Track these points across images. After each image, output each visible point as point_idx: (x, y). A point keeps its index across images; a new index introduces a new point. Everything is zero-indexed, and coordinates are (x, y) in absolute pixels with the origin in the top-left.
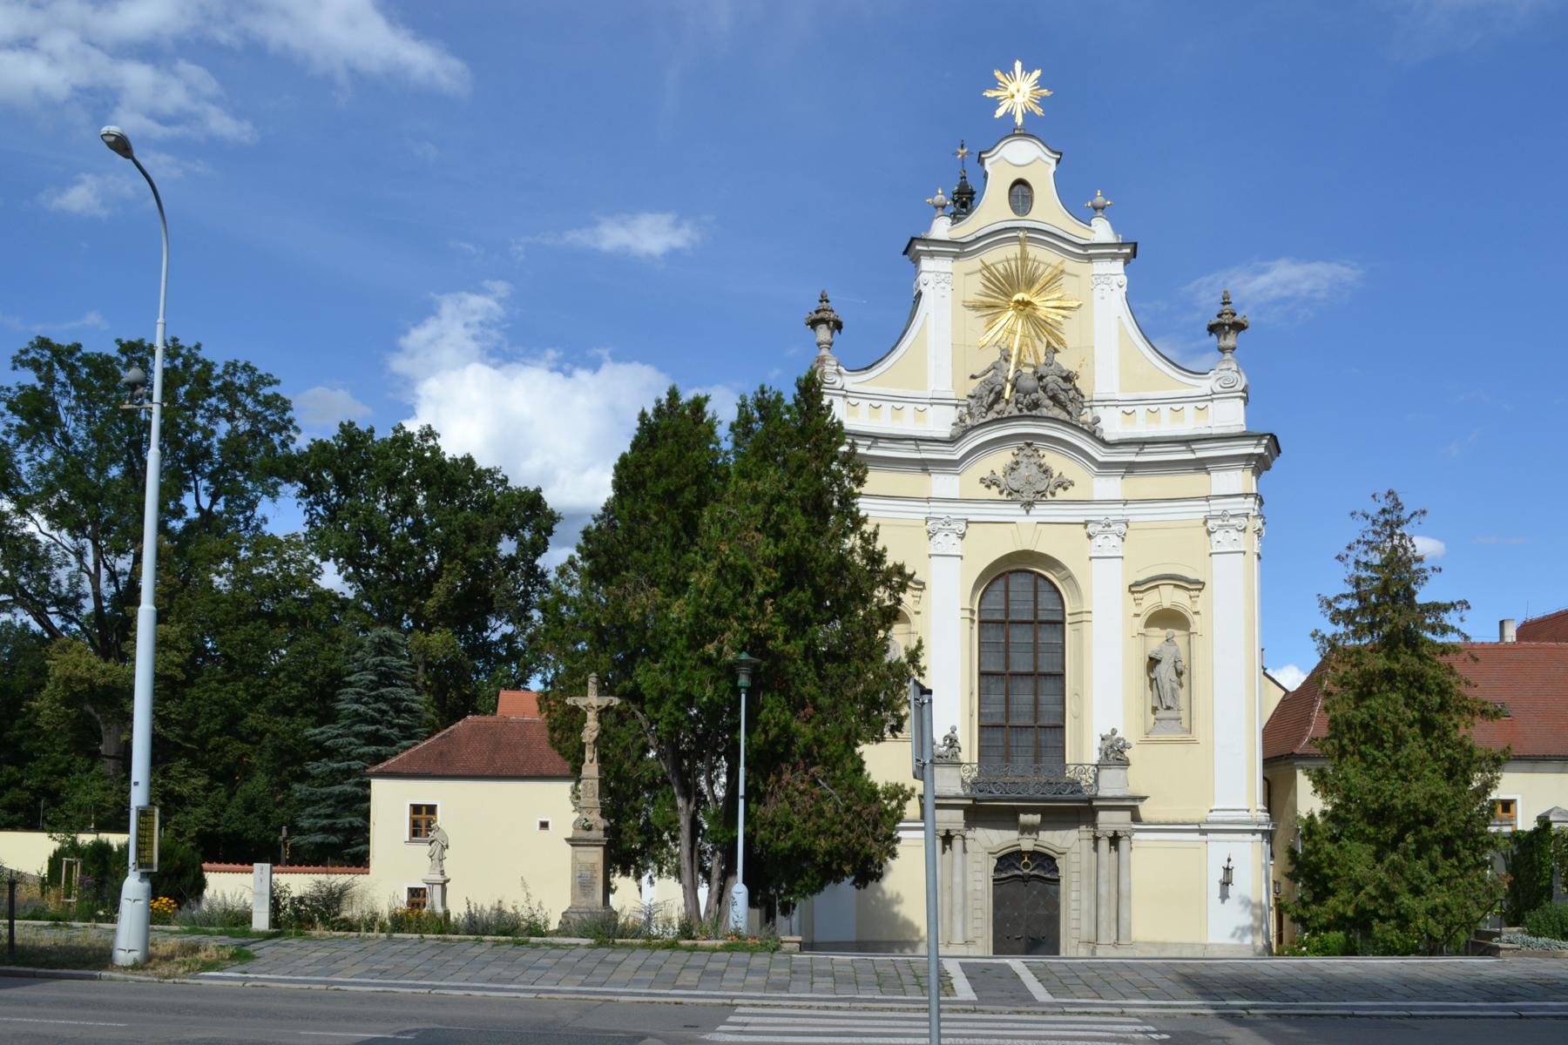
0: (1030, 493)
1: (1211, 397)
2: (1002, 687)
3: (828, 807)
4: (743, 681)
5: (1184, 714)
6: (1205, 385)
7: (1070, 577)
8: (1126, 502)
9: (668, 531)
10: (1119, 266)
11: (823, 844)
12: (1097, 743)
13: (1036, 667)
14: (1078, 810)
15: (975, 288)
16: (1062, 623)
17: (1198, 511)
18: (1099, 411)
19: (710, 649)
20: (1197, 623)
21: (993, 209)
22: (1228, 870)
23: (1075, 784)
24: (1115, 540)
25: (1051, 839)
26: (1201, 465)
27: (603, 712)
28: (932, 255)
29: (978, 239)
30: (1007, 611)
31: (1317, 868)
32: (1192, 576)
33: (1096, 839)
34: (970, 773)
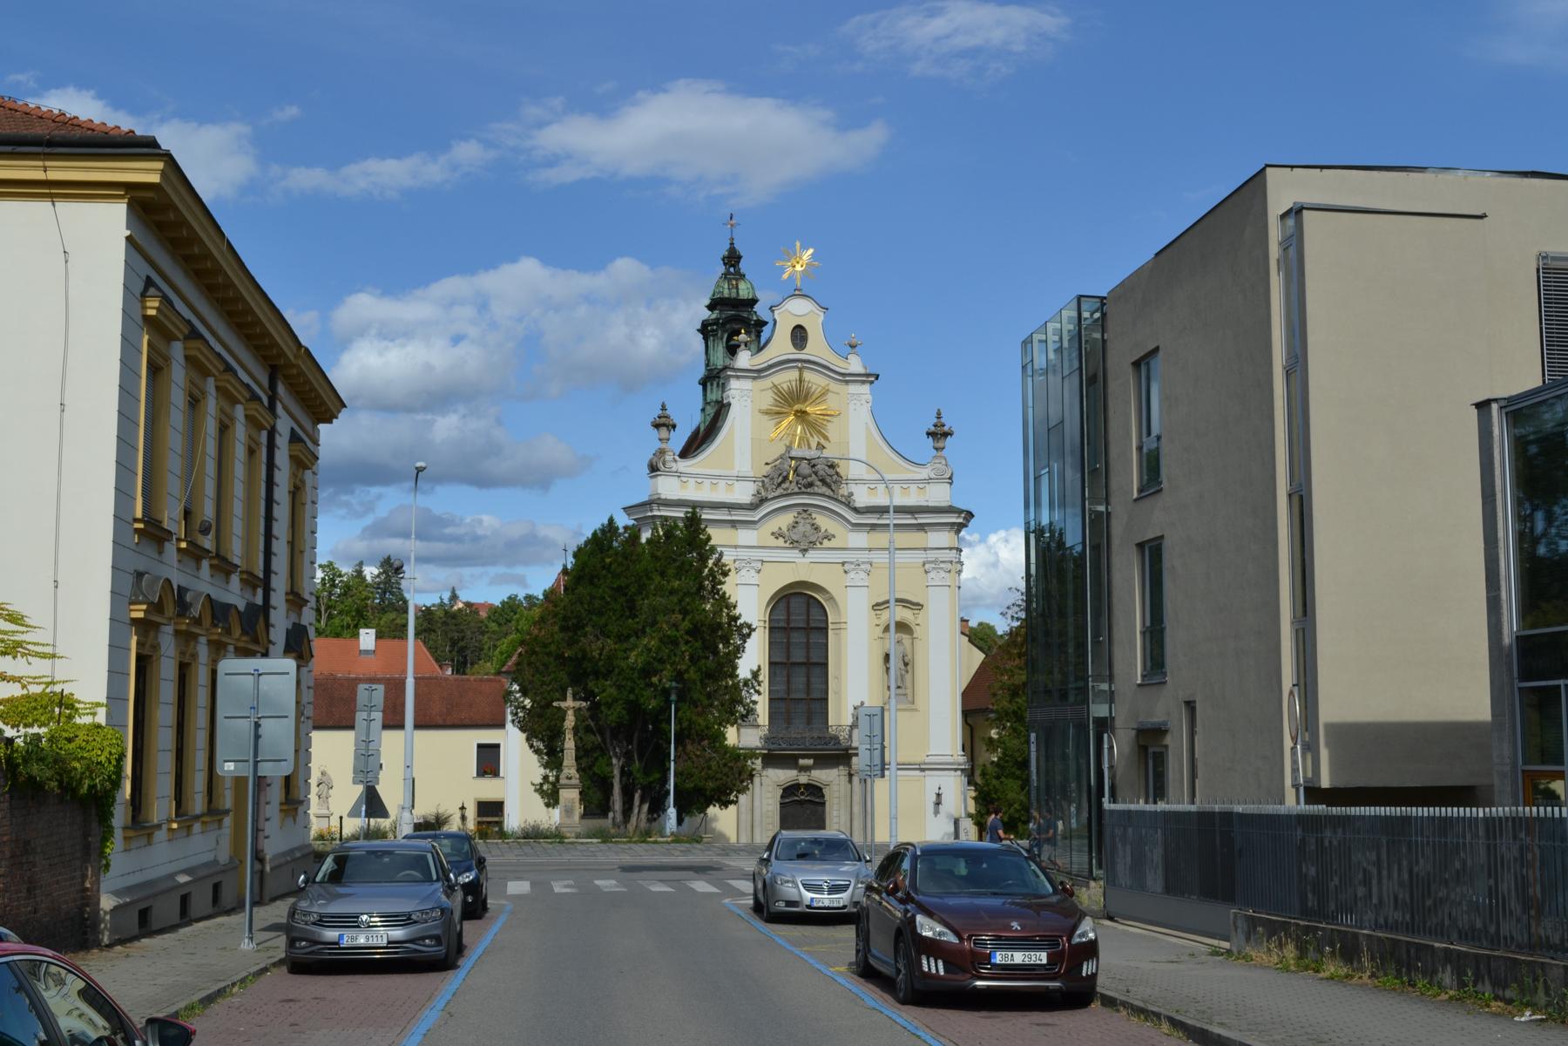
0: (805, 540)
1: (929, 480)
2: (785, 673)
3: (713, 764)
4: (673, 697)
5: (909, 691)
6: (924, 473)
7: (831, 599)
8: (870, 550)
9: (618, 607)
10: (866, 388)
11: (711, 784)
12: (851, 710)
13: (808, 657)
14: (840, 756)
15: (768, 400)
16: (826, 629)
17: (920, 557)
18: (853, 488)
19: (655, 680)
20: (918, 632)
21: (780, 346)
22: (939, 795)
23: (836, 738)
24: (863, 575)
25: (820, 775)
26: (921, 527)
27: (577, 711)
28: (738, 377)
29: (771, 367)
30: (788, 621)
31: (988, 793)
32: (915, 600)
33: (851, 775)
34: (765, 731)
